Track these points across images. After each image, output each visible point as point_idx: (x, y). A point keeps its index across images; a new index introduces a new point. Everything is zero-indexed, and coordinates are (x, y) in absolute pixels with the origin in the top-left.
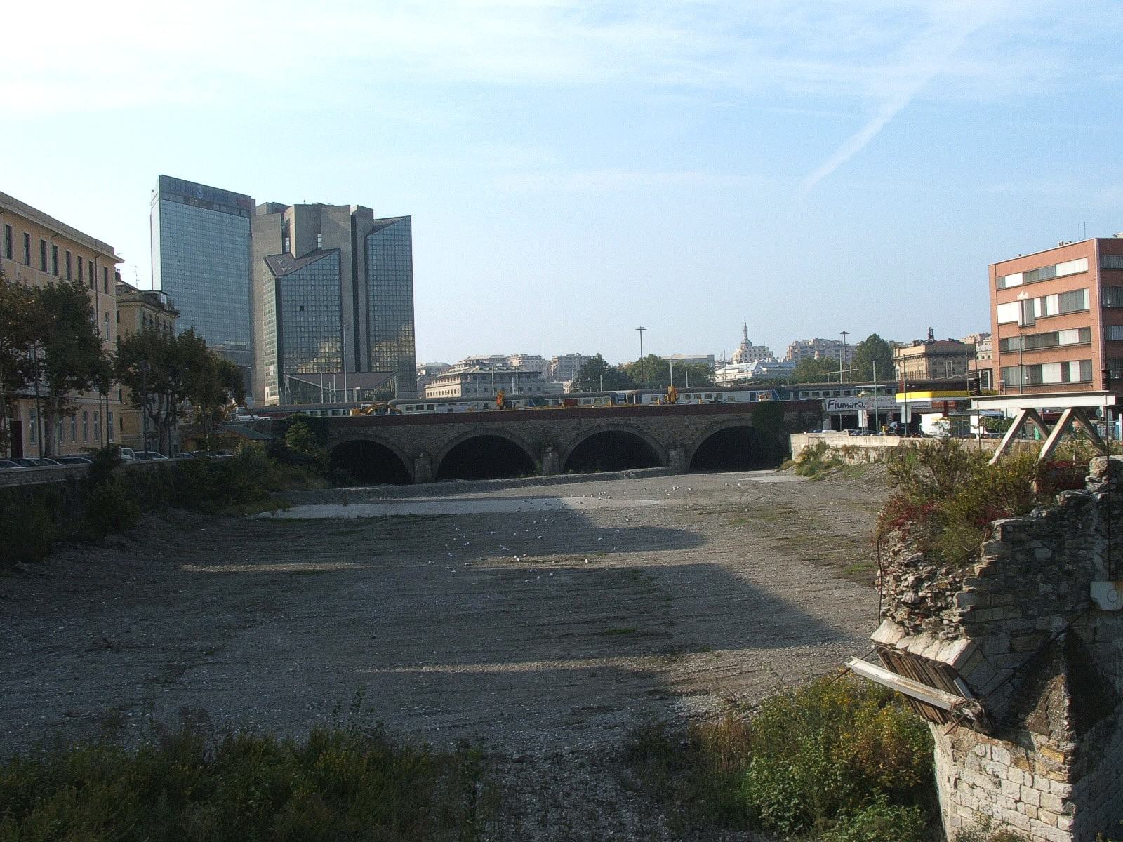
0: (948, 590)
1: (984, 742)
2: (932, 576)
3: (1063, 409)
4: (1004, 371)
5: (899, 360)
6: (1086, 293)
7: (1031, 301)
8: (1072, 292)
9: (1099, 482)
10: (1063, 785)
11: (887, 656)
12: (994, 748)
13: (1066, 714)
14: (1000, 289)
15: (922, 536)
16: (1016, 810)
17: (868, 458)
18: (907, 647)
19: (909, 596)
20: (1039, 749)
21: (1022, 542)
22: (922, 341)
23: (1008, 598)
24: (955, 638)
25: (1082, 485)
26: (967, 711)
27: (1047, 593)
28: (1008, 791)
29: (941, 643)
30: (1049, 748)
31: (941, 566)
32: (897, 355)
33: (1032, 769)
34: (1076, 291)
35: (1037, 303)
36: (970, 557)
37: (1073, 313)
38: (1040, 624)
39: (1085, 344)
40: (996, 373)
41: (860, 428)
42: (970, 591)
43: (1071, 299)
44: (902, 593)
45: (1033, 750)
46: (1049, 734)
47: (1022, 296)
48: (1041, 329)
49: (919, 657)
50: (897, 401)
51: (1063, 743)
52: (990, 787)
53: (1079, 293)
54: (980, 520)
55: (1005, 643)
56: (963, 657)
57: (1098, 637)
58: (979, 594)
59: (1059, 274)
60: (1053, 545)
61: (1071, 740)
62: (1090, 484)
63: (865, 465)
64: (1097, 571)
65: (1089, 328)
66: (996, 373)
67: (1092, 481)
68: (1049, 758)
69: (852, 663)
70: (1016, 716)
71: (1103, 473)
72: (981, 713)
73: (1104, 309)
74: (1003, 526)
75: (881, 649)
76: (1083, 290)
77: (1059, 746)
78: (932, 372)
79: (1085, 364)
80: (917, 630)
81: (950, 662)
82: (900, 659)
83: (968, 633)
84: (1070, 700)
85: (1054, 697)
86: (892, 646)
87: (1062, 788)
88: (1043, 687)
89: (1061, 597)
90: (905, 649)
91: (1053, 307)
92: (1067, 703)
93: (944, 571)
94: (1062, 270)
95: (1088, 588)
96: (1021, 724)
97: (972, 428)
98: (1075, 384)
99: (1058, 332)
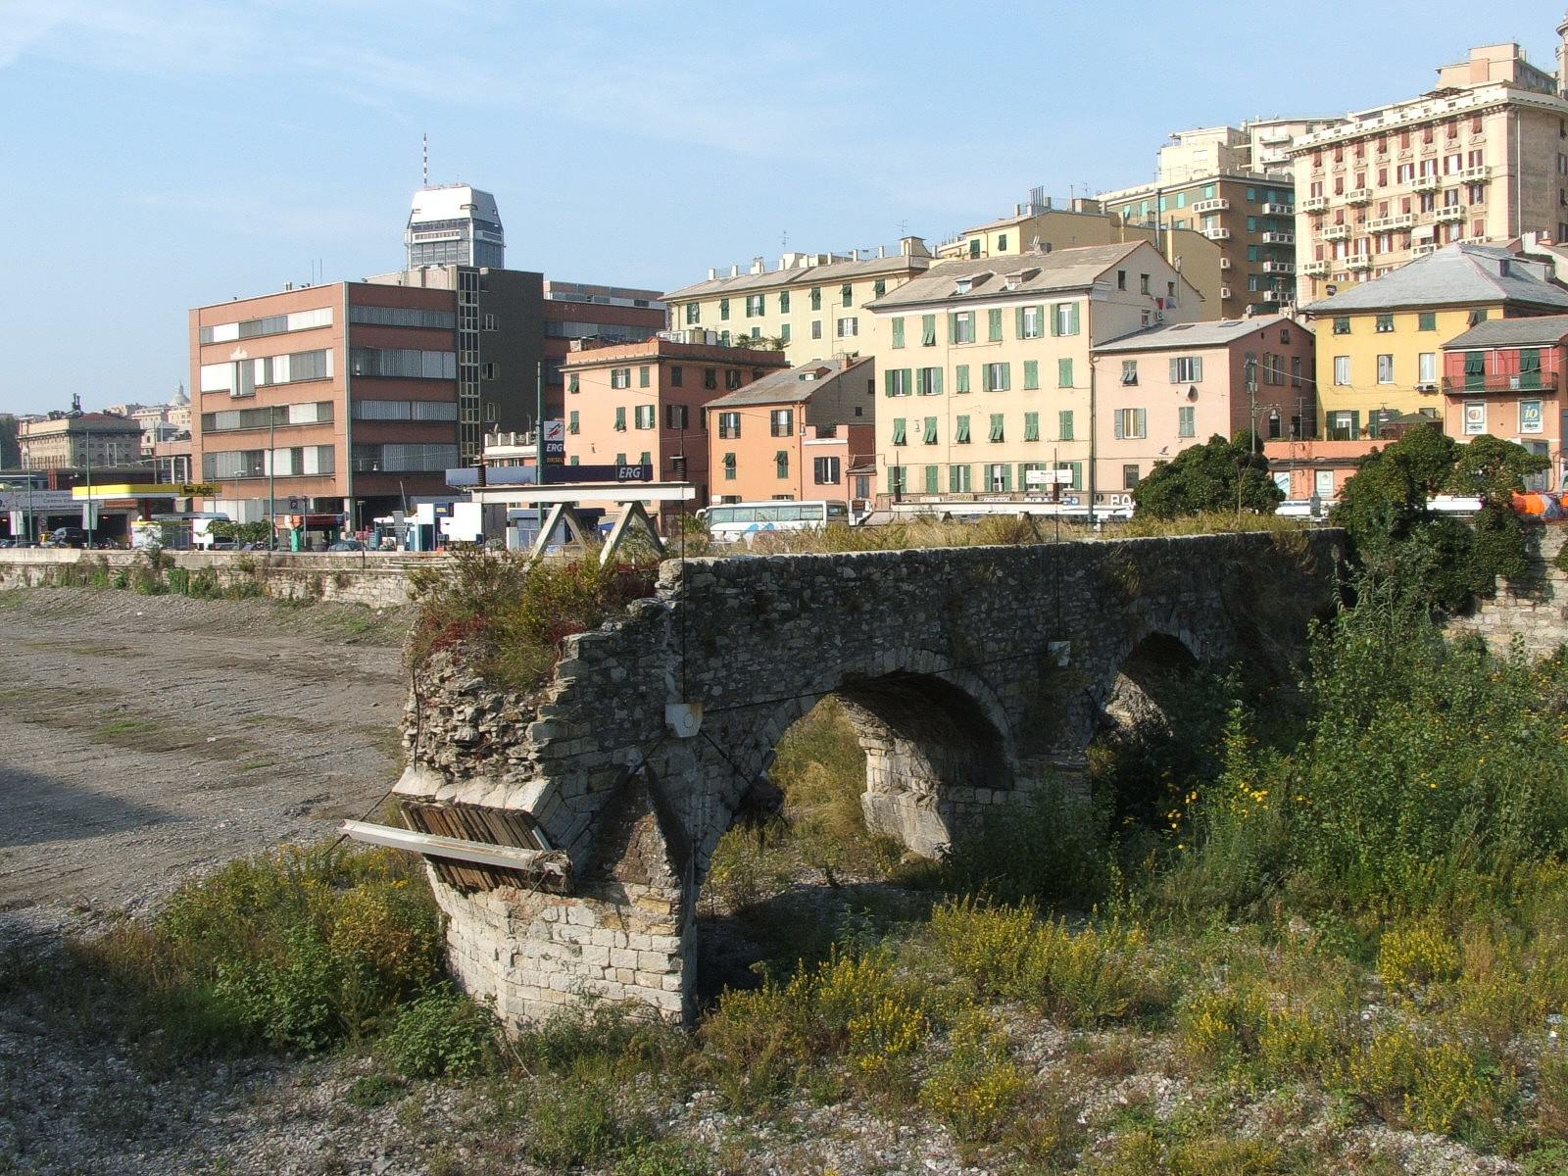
0: (518, 721)
1: (554, 904)
2: (498, 705)
3: (551, 505)
4: (209, 458)
5: (27, 439)
6: (329, 354)
7: (250, 361)
8: (311, 352)
9: (672, 589)
10: (670, 939)
11: (419, 814)
12: (570, 909)
13: (665, 858)
14: (205, 347)
15: (476, 657)
16: (604, 978)
17: (28, 580)
18: (455, 797)
19: (466, 733)
20: (636, 901)
21: (598, 661)
22: (63, 413)
23: (586, 727)
24: (528, 779)
25: (651, 592)
26: (549, 866)
27: (623, 721)
28: (592, 958)
29: (508, 787)
30: (650, 899)
31: (507, 693)
32: (25, 433)
33: (625, 926)
34: (314, 352)
35: (259, 365)
36: (538, 681)
37: (309, 381)
38: (617, 757)
39: (325, 423)
40: (197, 460)
41: (14, 537)
42: (548, 722)
43: (308, 364)
44: (455, 728)
45: (627, 903)
46: (649, 883)
47: (239, 354)
48: (265, 400)
49: (477, 808)
50: (74, 498)
51: (667, 891)
52: (566, 956)
53: (318, 354)
54: (550, 636)
55: (583, 780)
56: (543, 802)
57: (670, 771)
58: (559, 723)
59: (291, 328)
60: (628, 663)
61: (675, 886)
62: (661, 591)
63: (23, 590)
64: (669, 692)
65: (331, 402)
66: (197, 460)
67: (663, 587)
68: (650, 911)
69: (345, 827)
70: (600, 867)
71: (677, 578)
72: (569, 865)
73: (353, 378)
74: (581, 642)
75: (407, 804)
76: (325, 350)
77: (663, 895)
78: (79, 458)
79: (326, 451)
80: (467, 775)
81: (530, 810)
82: (441, 813)
83: (546, 773)
84: (666, 840)
85: (646, 840)
86: (430, 799)
87: (671, 943)
88: (630, 829)
89: (636, 724)
90: (451, 800)
91: (282, 371)
92: (664, 845)
93: (512, 698)
94: (295, 322)
95: (663, 714)
96: (608, 876)
97: (195, 536)
98: (311, 477)
99: (288, 407)
